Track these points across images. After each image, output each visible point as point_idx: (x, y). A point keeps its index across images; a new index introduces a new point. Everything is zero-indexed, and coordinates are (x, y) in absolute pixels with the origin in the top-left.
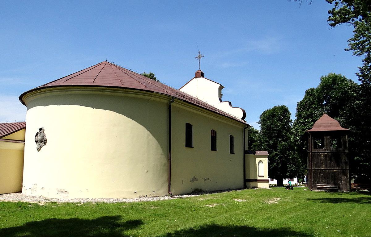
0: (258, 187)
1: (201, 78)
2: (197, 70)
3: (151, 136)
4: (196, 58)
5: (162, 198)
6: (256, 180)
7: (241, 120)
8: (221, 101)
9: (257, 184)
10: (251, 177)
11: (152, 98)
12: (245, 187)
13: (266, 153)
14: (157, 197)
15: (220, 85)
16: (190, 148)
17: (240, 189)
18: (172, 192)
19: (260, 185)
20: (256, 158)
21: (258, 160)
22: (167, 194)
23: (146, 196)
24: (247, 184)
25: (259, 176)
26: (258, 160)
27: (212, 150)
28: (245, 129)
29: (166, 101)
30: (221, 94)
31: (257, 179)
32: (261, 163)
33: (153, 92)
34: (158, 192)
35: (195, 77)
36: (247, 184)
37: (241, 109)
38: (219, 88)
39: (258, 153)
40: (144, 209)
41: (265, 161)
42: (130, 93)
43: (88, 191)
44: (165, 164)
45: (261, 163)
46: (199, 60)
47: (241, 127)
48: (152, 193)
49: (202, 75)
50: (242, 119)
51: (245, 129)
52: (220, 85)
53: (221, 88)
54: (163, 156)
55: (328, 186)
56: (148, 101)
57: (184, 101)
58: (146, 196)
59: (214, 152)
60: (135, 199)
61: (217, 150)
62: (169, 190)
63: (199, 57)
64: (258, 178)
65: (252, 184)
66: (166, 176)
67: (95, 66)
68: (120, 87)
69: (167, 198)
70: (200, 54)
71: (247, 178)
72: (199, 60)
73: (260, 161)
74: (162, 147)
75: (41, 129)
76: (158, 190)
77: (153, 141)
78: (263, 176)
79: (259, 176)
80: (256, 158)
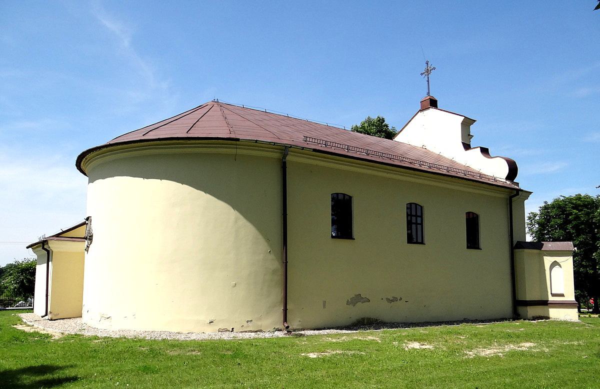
0: (551, 316)
1: (432, 111)
2: (424, 96)
3: (243, 221)
4: (422, 74)
5: (267, 335)
6: (545, 303)
7: (505, 181)
8: (467, 147)
9: (548, 310)
10: (529, 297)
11: (239, 151)
12: (516, 316)
13: (569, 245)
14: (256, 332)
15: (464, 118)
16: (343, 240)
17: (502, 319)
18: (294, 324)
19: (555, 314)
20: (544, 257)
21: (548, 261)
22: (281, 327)
23: (233, 329)
24: (521, 310)
25: (553, 295)
26: (548, 261)
27: (468, 247)
28: (511, 198)
29: (276, 155)
30: (469, 135)
31: (548, 301)
32: (556, 269)
33: (238, 140)
34: (259, 323)
35: (420, 111)
36: (521, 310)
37: (502, 157)
38: (463, 124)
39: (549, 246)
40: (574, 345)
41: (568, 263)
42: (198, 147)
43: (135, 318)
44: (274, 272)
45: (557, 266)
46: (428, 78)
47: (503, 196)
48: (245, 324)
49: (433, 103)
50: (508, 178)
51: (511, 198)
52: (464, 118)
53: (467, 123)
54: (272, 256)
55: (19, 327)
56: (235, 157)
57: (315, 150)
58: (233, 329)
59: (344, 243)
60: (209, 333)
61: (355, 237)
62: (285, 320)
63: (428, 72)
64: (551, 299)
65: (532, 311)
66: (278, 294)
67: (192, 111)
68: (227, 138)
69: (280, 334)
70: (429, 66)
71: (520, 297)
72: (428, 78)
73: (555, 264)
74: (268, 240)
75: (88, 219)
76: (260, 319)
77: (247, 229)
78: (562, 295)
79: (553, 295)
80: (544, 257)
